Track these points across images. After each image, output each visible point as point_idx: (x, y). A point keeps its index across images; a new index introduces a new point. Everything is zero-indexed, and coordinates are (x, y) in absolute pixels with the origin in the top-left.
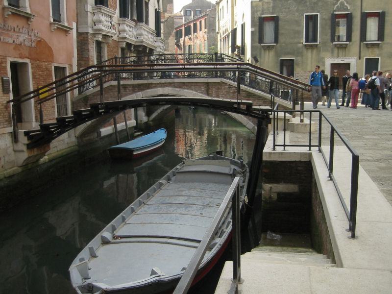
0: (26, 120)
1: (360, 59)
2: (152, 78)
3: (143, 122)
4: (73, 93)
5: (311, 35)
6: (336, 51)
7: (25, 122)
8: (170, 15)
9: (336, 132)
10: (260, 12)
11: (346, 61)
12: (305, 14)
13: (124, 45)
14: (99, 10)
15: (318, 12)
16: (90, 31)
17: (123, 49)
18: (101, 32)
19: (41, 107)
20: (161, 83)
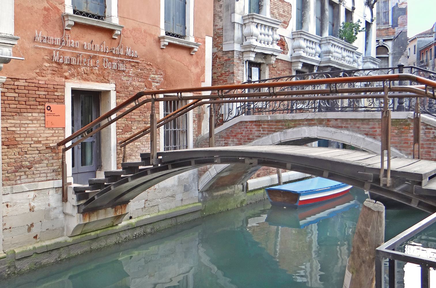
2: (355, 109)
8: (401, 29)
9: (392, 6)
13: (300, 67)
14: (251, 20)
16: (237, 47)
18: (252, 50)
20: (307, 120)
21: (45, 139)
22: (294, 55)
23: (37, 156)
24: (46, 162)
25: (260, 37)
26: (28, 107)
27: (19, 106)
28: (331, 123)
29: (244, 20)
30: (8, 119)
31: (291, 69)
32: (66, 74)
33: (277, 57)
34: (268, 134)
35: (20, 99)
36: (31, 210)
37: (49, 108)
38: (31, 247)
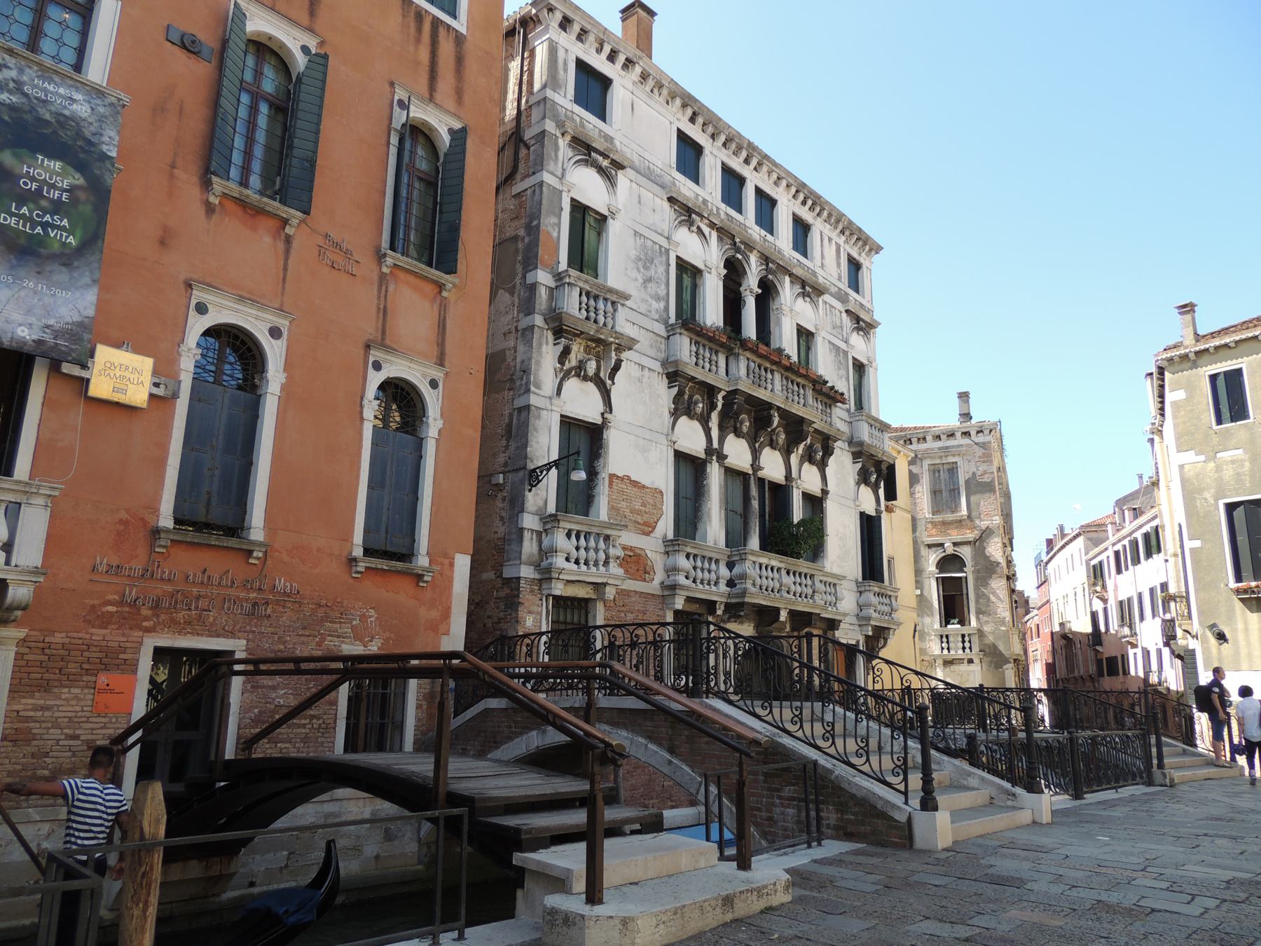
10: (1213, 491)
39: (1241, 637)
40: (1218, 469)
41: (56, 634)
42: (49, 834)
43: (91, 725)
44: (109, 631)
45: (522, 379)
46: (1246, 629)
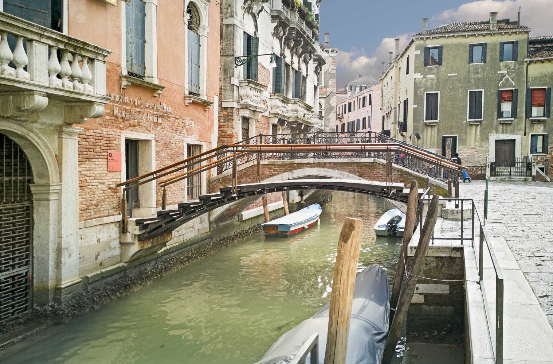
0: (144, 205)
1: (525, 135)
3: (295, 202)
4: (210, 173)
5: (475, 112)
6: (500, 127)
7: (143, 207)
10: (424, 89)
11: (511, 137)
12: (469, 91)
13: (275, 121)
15: (482, 89)
17: (274, 126)
19: (164, 190)
20: (309, 164)
21: (107, 181)
22: (272, 112)
23: (101, 195)
24: (108, 200)
25: (254, 98)
26: (95, 154)
27: (89, 153)
28: (328, 165)
29: (240, 83)
30: (82, 164)
31: (269, 123)
32: (121, 126)
33: (263, 114)
34: (278, 174)
35: (89, 147)
36: (99, 241)
37: (110, 155)
38: (99, 272)
39: (425, 138)
40: (426, 81)
41: (90, 131)
42: (100, 231)
43: (108, 178)
44: (108, 129)
45: (228, 9)
46: (427, 136)
